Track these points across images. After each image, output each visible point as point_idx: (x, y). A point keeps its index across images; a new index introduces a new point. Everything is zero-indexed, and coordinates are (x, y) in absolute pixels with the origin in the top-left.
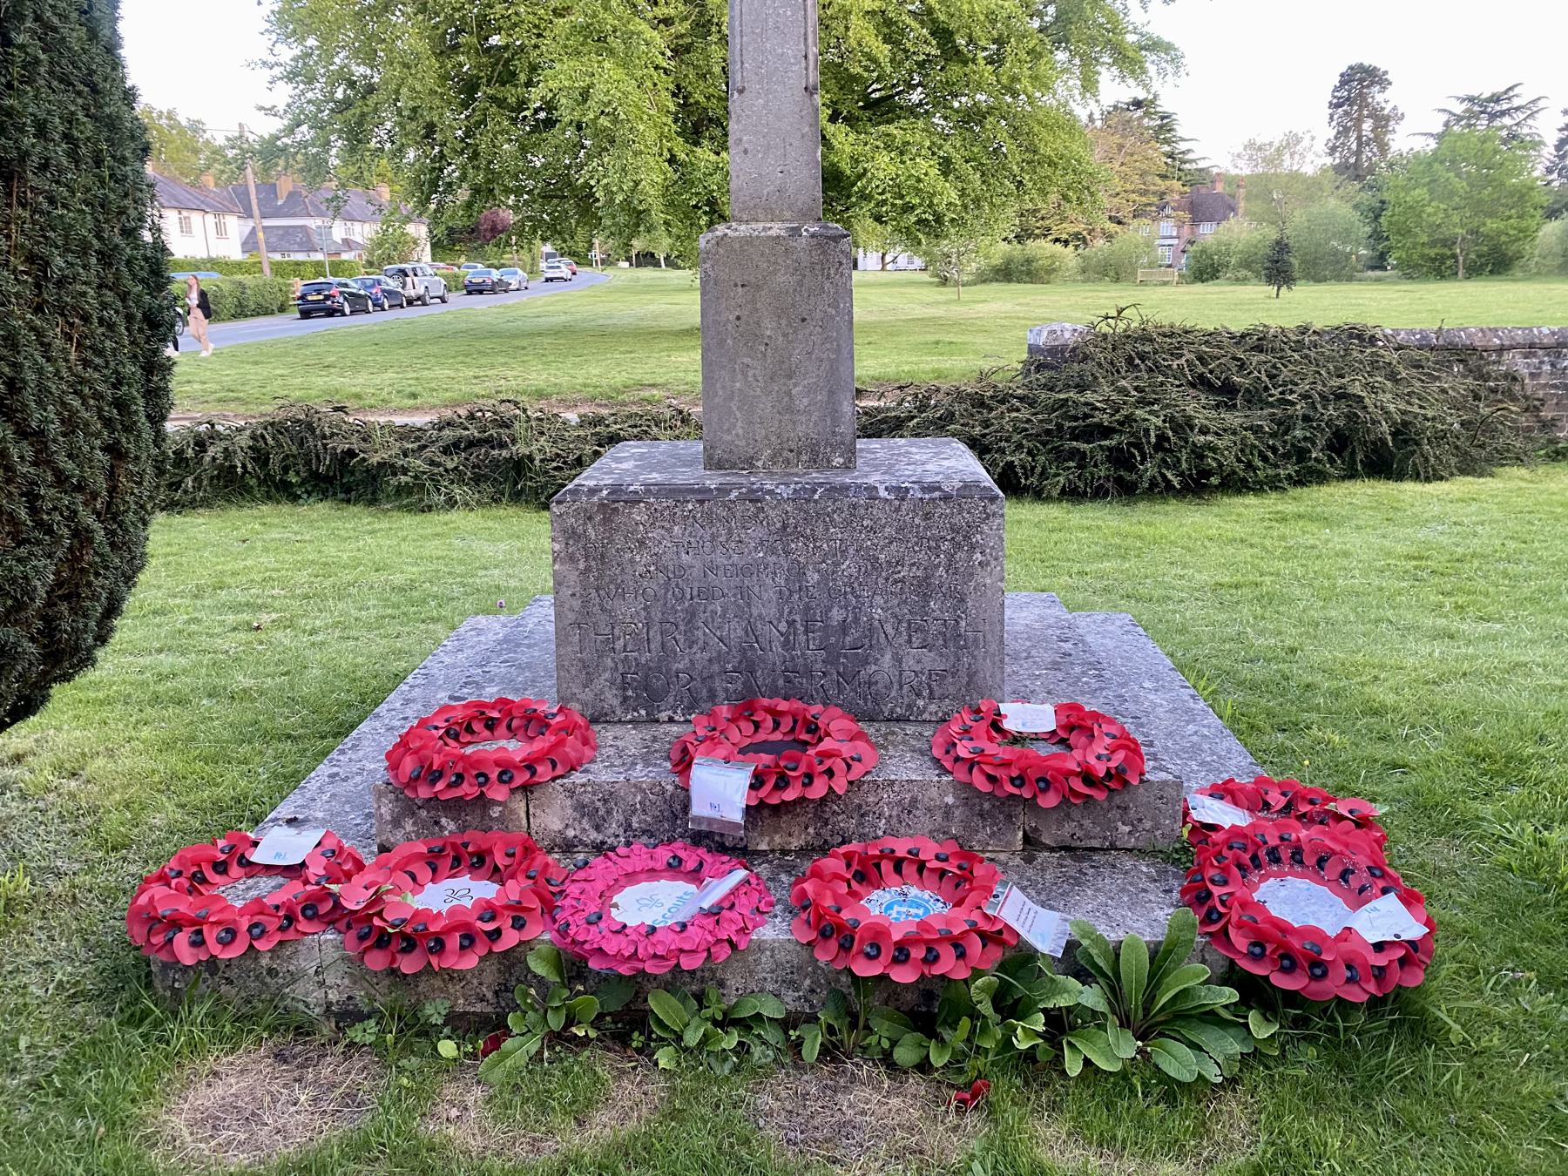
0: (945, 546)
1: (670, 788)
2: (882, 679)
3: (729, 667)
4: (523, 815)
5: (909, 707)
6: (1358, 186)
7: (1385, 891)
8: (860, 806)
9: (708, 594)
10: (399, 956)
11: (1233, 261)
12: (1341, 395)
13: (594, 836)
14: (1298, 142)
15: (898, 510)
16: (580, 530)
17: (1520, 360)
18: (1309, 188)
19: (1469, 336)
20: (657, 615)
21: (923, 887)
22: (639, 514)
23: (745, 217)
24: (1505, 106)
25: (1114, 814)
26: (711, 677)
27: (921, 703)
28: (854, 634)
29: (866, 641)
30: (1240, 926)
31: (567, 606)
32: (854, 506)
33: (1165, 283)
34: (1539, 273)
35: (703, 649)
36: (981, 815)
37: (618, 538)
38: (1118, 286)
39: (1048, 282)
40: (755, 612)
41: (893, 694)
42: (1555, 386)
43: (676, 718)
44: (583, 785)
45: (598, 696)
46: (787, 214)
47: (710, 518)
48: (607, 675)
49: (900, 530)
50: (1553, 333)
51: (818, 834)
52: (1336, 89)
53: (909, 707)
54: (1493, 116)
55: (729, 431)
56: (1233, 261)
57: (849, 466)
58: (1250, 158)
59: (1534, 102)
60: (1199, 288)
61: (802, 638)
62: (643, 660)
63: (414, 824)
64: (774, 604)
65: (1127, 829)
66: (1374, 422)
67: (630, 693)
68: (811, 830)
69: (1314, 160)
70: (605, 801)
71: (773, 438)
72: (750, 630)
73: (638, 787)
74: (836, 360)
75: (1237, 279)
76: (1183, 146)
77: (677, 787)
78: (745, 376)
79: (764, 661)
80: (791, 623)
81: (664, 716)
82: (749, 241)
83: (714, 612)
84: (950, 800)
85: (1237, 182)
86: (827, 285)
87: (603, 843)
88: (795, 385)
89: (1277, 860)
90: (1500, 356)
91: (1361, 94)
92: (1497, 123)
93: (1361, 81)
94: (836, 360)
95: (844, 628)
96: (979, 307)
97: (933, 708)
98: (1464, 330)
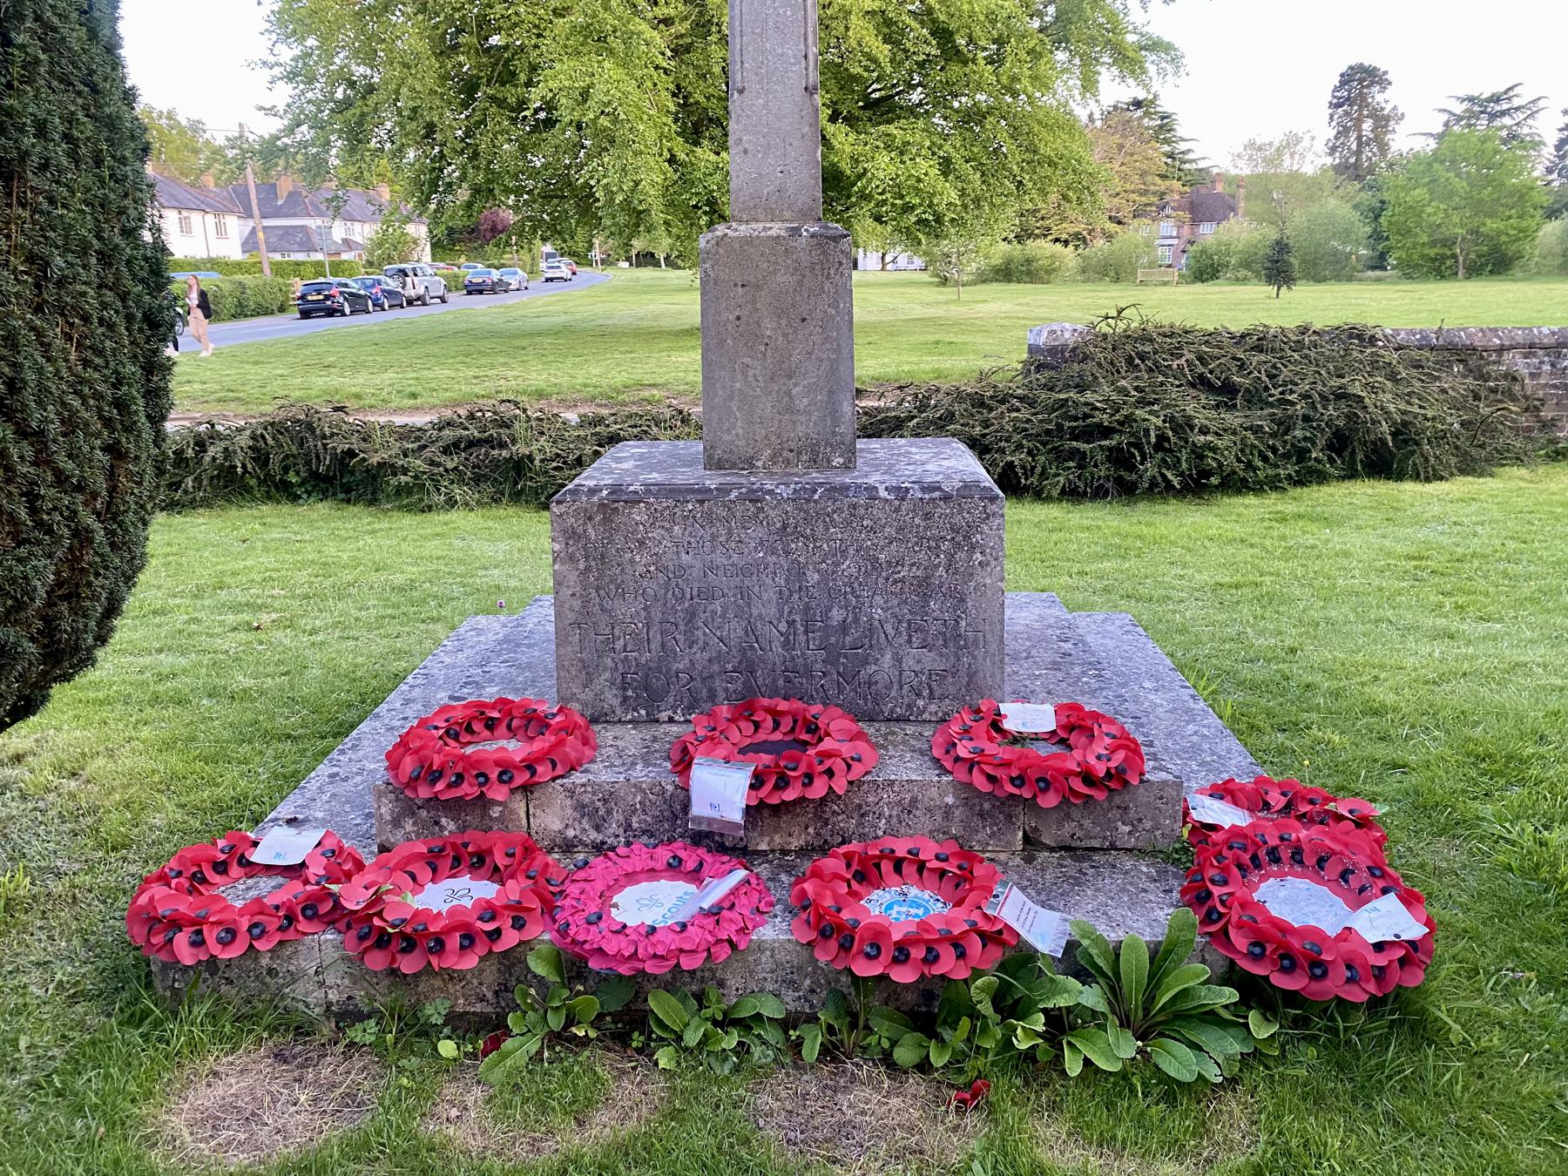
1: (670, 788)
3: (729, 667)
4: (523, 815)
5: (909, 707)
7: (1385, 891)
8: (860, 806)
10: (399, 957)
11: (1233, 261)
12: (1341, 395)
13: (594, 835)
14: (1298, 142)
15: (898, 510)
16: (580, 530)
17: (1520, 360)
18: (1310, 188)
19: (1469, 336)
20: (657, 616)
21: (923, 888)
22: (639, 514)
24: (1505, 106)
25: (1114, 814)
26: (711, 677)
27: (921, 703)
28: (854, 634)
29: (866, 641)
31: (567, 606)
33: (1165, 284)
34: (1539, 273)
35: (703, 649)
36: (981, 815)
37: (619, 538)
39: (1048, 283)
40: (755, 612)
41: (893, 694)
42: (1555, 386)
43: (676, 718)
44: (583, 785)
47: (710, 518)
48: (607, 675)
49: (900, 529)
50: (1553, 333)
52: (1336, 89)
53: (909, 707)
54: (1493, 116)
55: (729, 431)
56: (1233, 261)
57: (849, 466)
58: (1250, 158)
59: (1534, 102)
60: (1198, 288)
65: (1127, 829)
66: (1374, 422)
68: (811, 830)
69: (1314, 160)
70: (605, 801)
71: (773, 438)
72: (750, 630)
74: (836, 360)
75: (1237, 279)
76: (1183, 146)
78: (745, 375)
79: (763, 661)
80: (791, 623)
81: (664, 716)
82: (748, 241)
83: (714, 612)
85: (1237, 182)
87: (603, 843)
88: (795, 385)
89: (1277, 860)
90: (1500, 356)
91: (1361, 94)
92: (1497, 123)
93: (1361, 81)
94: (836, 360)
95: (844, 628)
97: (933, 708)
98: (1464, 330)
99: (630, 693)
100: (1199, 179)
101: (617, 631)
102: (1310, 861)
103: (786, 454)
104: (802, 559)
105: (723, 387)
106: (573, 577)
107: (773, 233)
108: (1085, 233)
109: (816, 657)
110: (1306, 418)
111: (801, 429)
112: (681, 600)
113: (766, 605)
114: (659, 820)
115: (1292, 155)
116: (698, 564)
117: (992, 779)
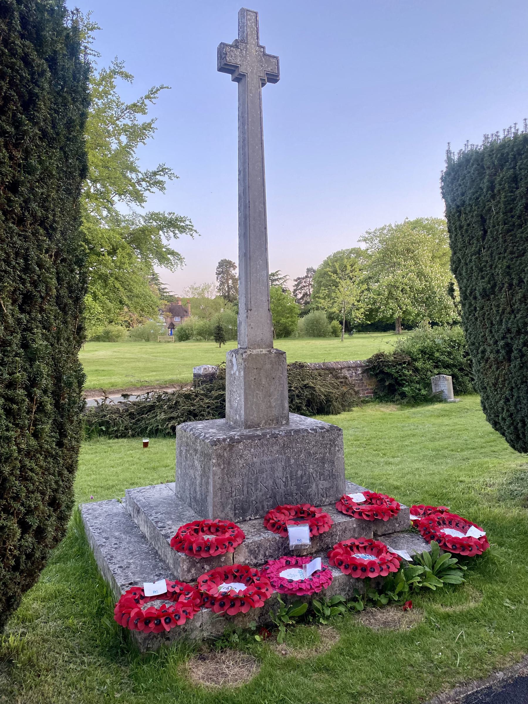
1: (278, 538)
2: (313, 493)
3: (268, 496)
4: (232, 558)
5: (321, 501)
6: (232, 304)
7: (470, 527)
8: (331, 533)
9: (261, 471)
11: (195, 332)
12: (306, 386)
13: (255, 561)
14: (209, 287)
15: (315, 436)
16: (222, 454)
17: (346, 372)
18: (215, 305)
20: (246, 481)
21: (361, 553)
22: (241, 446)
24: (276, 278)
25: (394, 521)
26: (263, 501)
27: (324, 499)
28: (305, 478)
29: (308, 481)
32: (303, 436)
33: (169, 342)
34: (299, 336)
35: (260, 491)
36: (363, 529)
37: (234, 455)
38: (148, 343)
39: (117, 341)
40: (276, 476)
41: (316, 497)
42: (357, 380)
43: (252, 518)
44: (251, 543)
45: (227, 515)
46: (264, 346)
47: (262, 445)
48: (229, 506)
49: (316, 442)
50: (354, 363)
51: (320, 545)
52: (218, 268)
53: (321, 501)
54: (273, 281)
55: (252, 416)
56: (195, 332)
57: (287, 423)
58: (192, 293)
59: (285, 277)
60: (183, 344)
61: (290, 482)
62: (241, 499)
63: (195, 570)
64: (281, 472)
65: (398, 525)
66: (319, 395)
67: (237, 512)
68: (318, 545)
69: (213, 294)
70: (258, 547)
71: (265, 417)
72: (275, 482)
73: (268, 540)
74: (283, 390)
75: (198, 340)
76: (163, 286)
78: (257, 397)
80: (287, 478)
81: (248, 518)
82: (257, 355)
83: (263, 477)
84: (355, 526)
85: (188, 301)
86: (280, 368)
87: (257, 563)
88: (272, 399)
89: (445, 524)
90: (341, 371)
91: (227, 270)
92: (274, 283)
93: (226, 266)
94: (283, 390)
95: (302, 477)
97: (327, 500)
98: (330, 362)
99: (237, 512)
100: (171, 299)
101: (233, 489)
102: (447, 523)
103: (269, 421)
104: (289, 455)
105: (250, 401)
106: (219, 471)
107: (264, 352)
108: (129, 321)
109: (293, 488)
110: (298, 396)
111: (273, 413)
113: (279, 474)
115: (208, 292)
116: (259, 461)
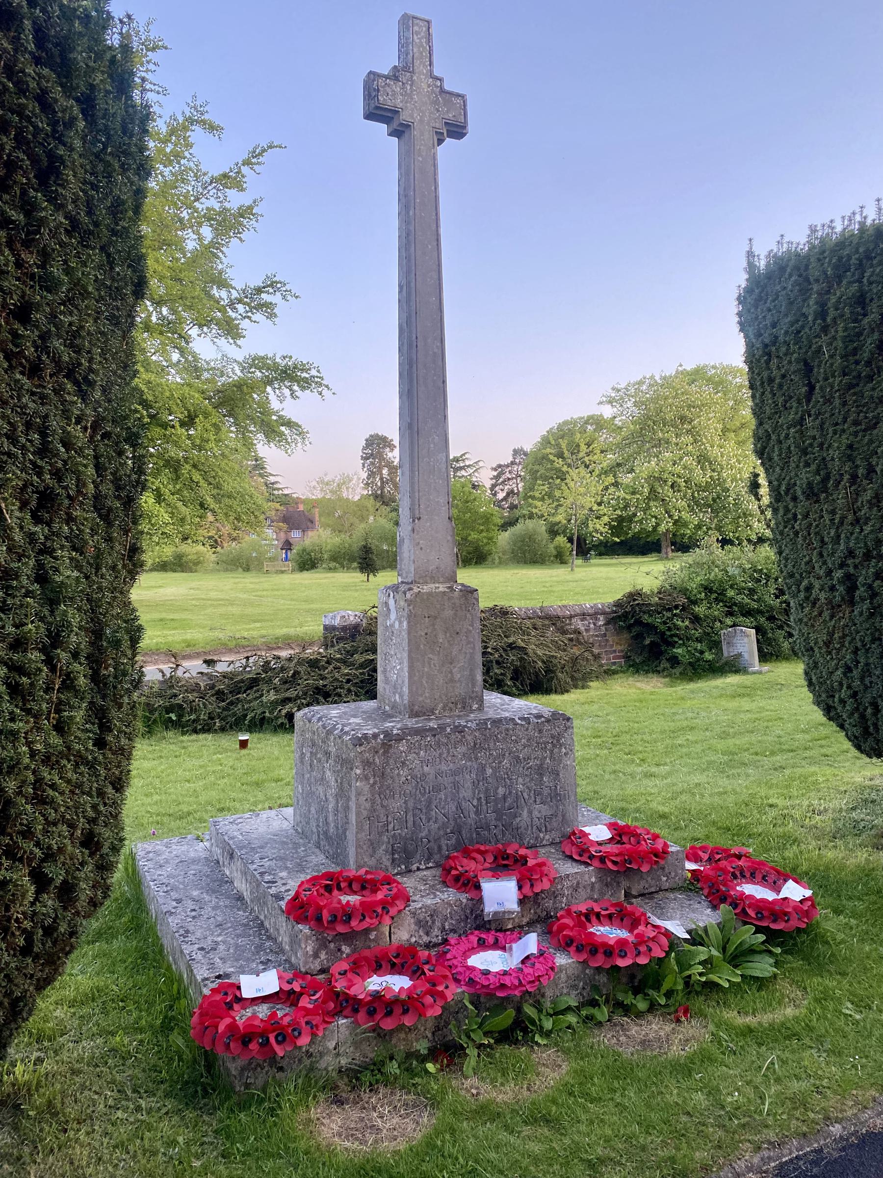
0: (549, 746)
1: (464, 901)
2: (523, 825)
3: (448, 830)
5: (537, 838)
6: (388, 509)
7: (785, 881)
8: (554, 892)
10: (402, 1018)
11: (326, 556)
12: (512, 646)
13: (426, 939)
14: (350, 481)
15: (527, 729)
16: (371, 760)
17: (579, 622)
18: (360, 511)
19: (554, 610)
20: (411, 804)
21: (604, 926)
22: (403, 747)
23: (421, 581)
24: (462, 465)
25: (660, 872)
26: (439, 838)
27: (542, 835)
28: (509, 800)
29: (515, 804)
30: (750, 906)
31: (363, 807)
34: (500, 563)
35: (435, 822)
36: (607, 885)
37: (391, 761)
38: (247, 574)
39: (196, 571)
40: (461, 796)
41: (529, 832)
42: (597, 636)
43: (421, 867)
44: (420, 908)
45: (379, 861)
47: (438, 744)
48: (384, 847)
49: (528, 740)
52: (364, 449)
53: (537, 838)
54: (457, 470)
55: (421, 695)
56: (326, 556)
57: (481, 708)
59: (476, 463)
60: (306, 575)
61: (485, 807)
63: (327, 953)
65: (665, 879)
67: (396, 856)
68: (532, 911)
69: (357, 492)
70: (432, 916)
71: (444, 697)
72: (459, 807)
75: (330, 569)
76: (272, 479)
77: (468, 899)
78: (429, 664)
79: (466, 824)
80: (479, 799)
81: (414, 867)
82: (430, 594)
83: (441, 799)
84: (593, 880)
85: (315, 504)
86: (468, 615)
87: (430, 942)
88: (455, 667)
89: (744, 877)
90: (570, 620)
91: (379, 452)
92: (458, 474)
93: (378, 445)
95: (505, 798)
96: (161, 590)
97: (547, 837)
99: (396, 856)
100: (286, 500)
102: (748, 875)
103: (450, 705)
105: (419, 671)
112: (423, 795)
113: (466, 793)
114: (459, 921)
116: (433, 772)
117: (615, 863)
